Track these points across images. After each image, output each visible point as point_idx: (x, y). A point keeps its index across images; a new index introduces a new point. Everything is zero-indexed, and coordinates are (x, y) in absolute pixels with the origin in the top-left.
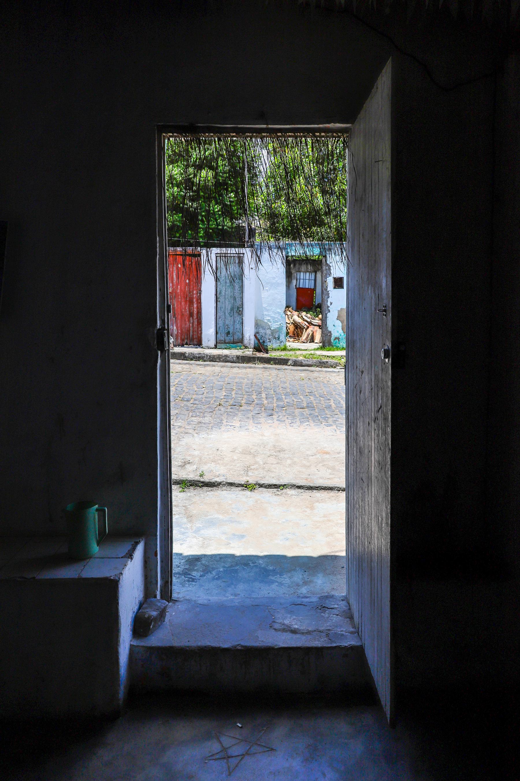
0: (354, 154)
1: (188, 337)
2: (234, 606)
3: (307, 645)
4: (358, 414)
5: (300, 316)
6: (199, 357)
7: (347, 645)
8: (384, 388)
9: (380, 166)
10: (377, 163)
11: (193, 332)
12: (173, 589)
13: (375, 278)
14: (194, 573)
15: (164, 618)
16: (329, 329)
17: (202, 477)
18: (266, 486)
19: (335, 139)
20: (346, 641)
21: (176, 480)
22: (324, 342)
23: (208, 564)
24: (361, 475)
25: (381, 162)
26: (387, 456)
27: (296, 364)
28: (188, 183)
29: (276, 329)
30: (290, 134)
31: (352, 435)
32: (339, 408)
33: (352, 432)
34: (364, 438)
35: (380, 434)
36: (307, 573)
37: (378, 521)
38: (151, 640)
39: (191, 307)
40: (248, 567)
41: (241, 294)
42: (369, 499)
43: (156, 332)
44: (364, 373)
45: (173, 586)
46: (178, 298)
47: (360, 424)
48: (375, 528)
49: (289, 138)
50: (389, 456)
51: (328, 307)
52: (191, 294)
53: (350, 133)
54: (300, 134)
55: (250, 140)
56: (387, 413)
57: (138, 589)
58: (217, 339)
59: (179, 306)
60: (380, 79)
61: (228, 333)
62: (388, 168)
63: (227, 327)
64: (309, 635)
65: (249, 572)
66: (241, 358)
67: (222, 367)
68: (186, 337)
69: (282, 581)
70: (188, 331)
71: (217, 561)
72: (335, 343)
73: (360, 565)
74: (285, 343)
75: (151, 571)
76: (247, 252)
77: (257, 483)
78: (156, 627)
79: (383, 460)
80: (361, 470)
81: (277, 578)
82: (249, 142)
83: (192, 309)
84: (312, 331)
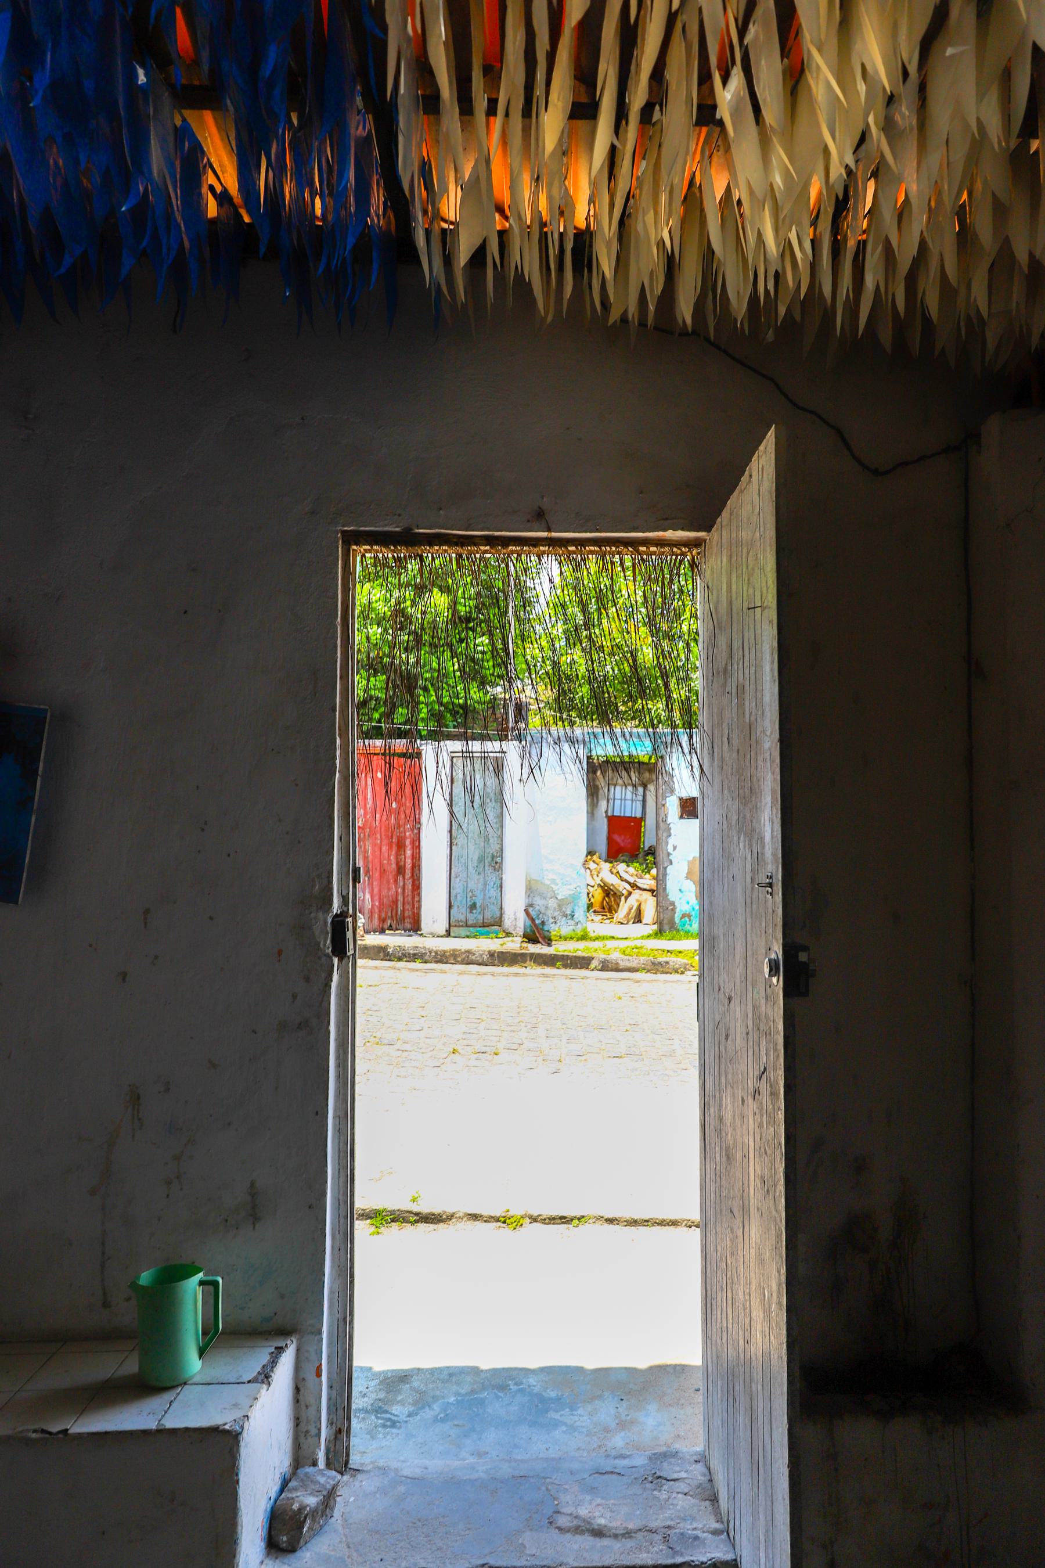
0: (710, 587)
1: (394, 914)
2: (476, 1480)
3: (625, 1563)
4: (724, 1081)
5: (615, 871)
6: (415, 955)
7: (705, 1560)
8: (770, 1034)
9: (758, 616)
10: (753, 610)
11: (404, 904)
12: (351, 1444)
13: (751, 821)
14: (396, 1409)
15: (332, 1510)
16: (671, 898)
17: (415, 1203)
18: (545, 1219)
19: (677, 558)
20: (703, 1551)
21: (363, 1210)
22: (660, 923)
23: (424, 1389)
24: (730, 1203)
25: (759, 609)
26: (778, 1168)
27: (606, 966)
28: (399, 617)
29: (567, 898)
30: (592, 548)
31: (710, 1121)
32: (690, 1056)
33: (713, 1115)
34: (735, 1129)
35: (765, 1123)
36: (624, 1404)
37: (763, 1298)
38: (305, 1561)
39: (401, 855)
40: (506, 1393)
41: (500, 830)
42: (746, 1251)
43: (330, 920)
44: (732, 1002)
45: (351, 1438)
46: (376, 839)
47: (727, 1101)
48: (757, 1313)
49: (590, 556)
50: (781, 1168)
51: (669, 854)
52: (402, 829)
53: (703, 548)
54: (611, 548)
55: (517, 559)
56: (777, 1083)
57: (279, 1449)
58: (452, 918)
59: (378, 853)
60: (755, 460)
61: (473, 907)
62: (771, 622)
63: (471, 894)
64: (627, 1540)
65: (508, 1405)
66: (498, 955)
67: (460, 974)
68: (390, 914)
69: (575, 1422)
70: (393, 902)
71: (443, 1382)
73: (731, 1386)
74: (584, 925)
75: (307, 1407)
76: (512, 749)
77: (526, 1214)
78: (315, 1532)
79: (771, 1176)
80: (729, 1191)
81: (564, 1415)
82: (515, 562)
83: (403, 859)
84: (638, 901)
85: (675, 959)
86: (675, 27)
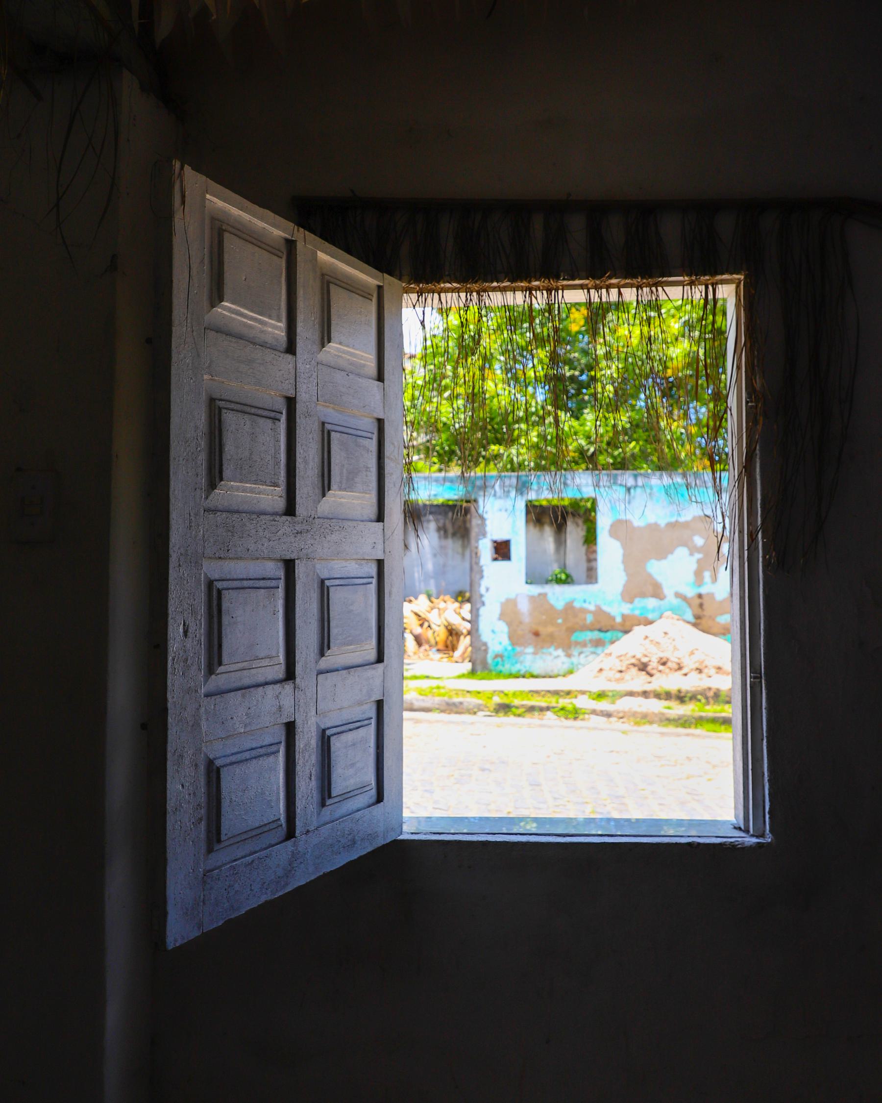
51: (481, 596)
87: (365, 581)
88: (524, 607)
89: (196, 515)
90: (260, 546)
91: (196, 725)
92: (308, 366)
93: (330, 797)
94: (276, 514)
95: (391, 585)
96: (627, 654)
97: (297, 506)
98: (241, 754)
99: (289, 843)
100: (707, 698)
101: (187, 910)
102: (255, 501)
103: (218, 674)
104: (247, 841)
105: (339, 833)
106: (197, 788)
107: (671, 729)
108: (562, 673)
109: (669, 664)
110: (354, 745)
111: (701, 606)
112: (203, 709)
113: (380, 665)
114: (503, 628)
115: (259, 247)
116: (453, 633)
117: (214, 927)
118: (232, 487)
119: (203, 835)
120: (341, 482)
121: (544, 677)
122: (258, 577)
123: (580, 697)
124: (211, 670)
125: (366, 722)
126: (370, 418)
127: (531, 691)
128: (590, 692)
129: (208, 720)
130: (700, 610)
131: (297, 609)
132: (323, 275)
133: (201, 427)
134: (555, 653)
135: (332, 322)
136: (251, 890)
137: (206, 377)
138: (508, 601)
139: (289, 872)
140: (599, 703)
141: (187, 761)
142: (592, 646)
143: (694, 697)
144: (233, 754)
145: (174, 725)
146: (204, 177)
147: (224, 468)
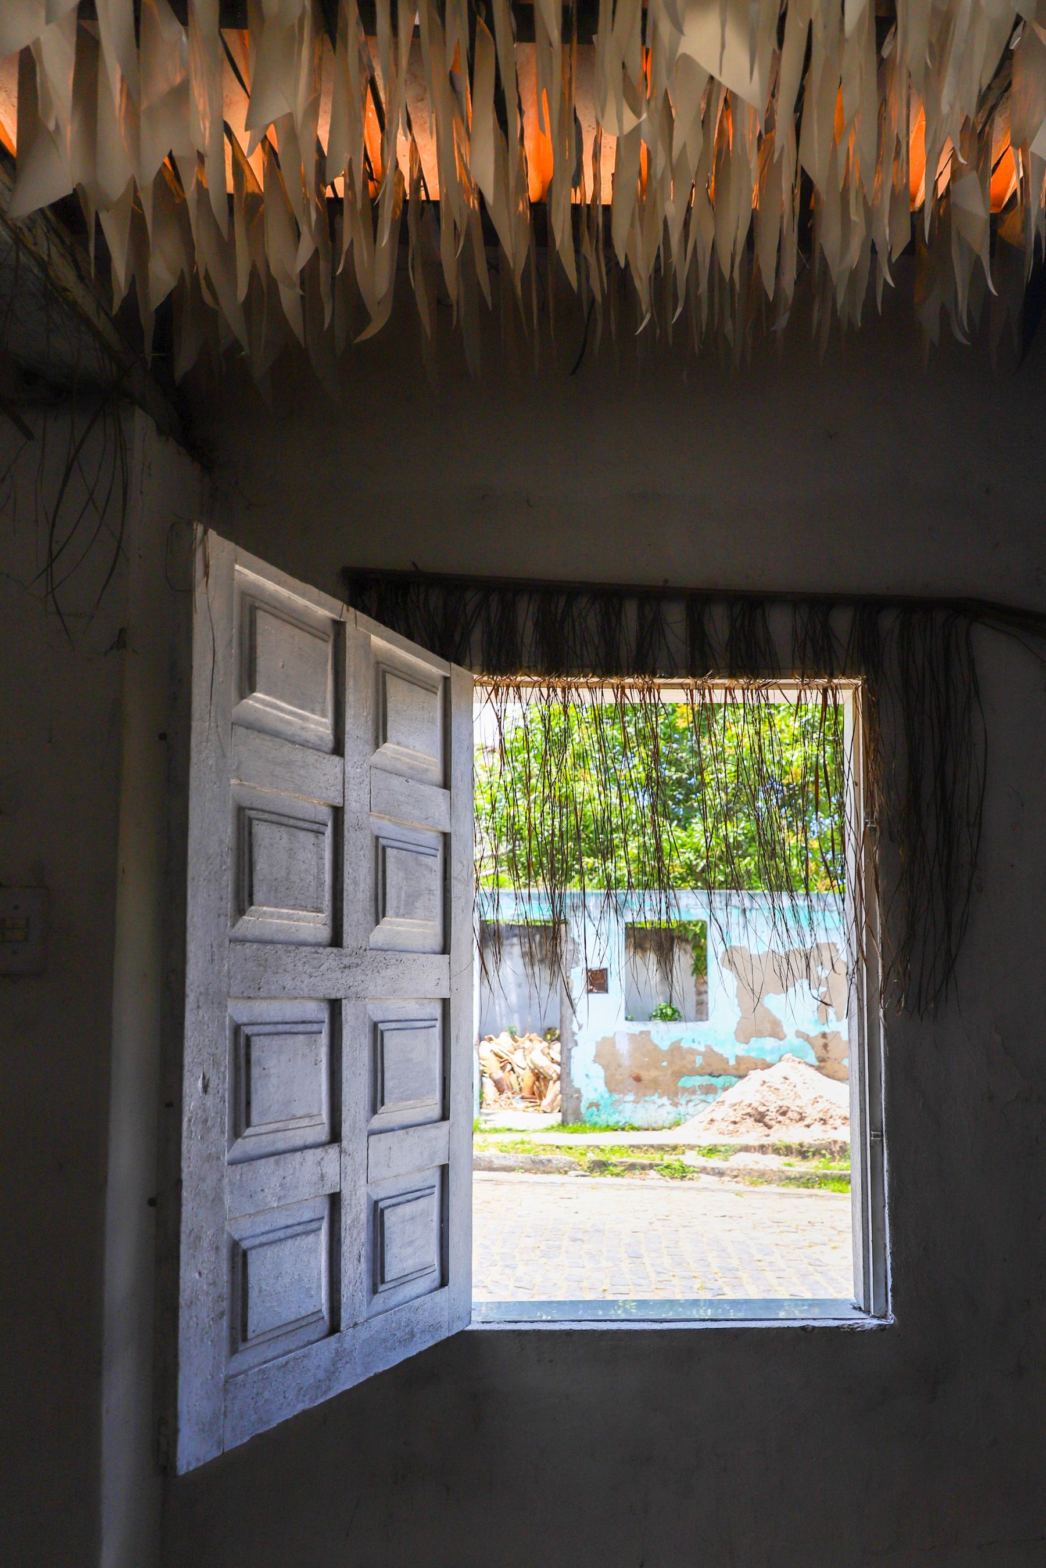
16: (577, 1084)
51: (574, 1034)
72: (589, 1114)
85: (559, 1157)
86: (560, 27)
87: (427, 1024)
88: (623, 1047)
89: (220, 946)
90: (299, 983)
91: (218, 1200)
92: (359, 770)
93: (383, 1282)
94: (318, 945)
95: (459, 1028)
96: (742, 1101)
97: (345, 936)
98: (275, 1233)
99: (333, 1339)
100: (832, 1153)
101: (204, 1425)
102: (293, 930)
103: (246, 1137)
104: (280, 1338)
105: (394, 1325)
106: (218, 1276)
107: (792, 1189)
108: (667, 1124)
109: (790, 1114)
110: (413, 1218)
111: (825, 1046)
112: (226, 1180)
113: (445, 1124)
114: (598, 1073)
115: (300, 629)
116: (539, 1076)
117: (238, 1444)
118: (265, 913)
119: (225, 1333)
120: (398, 907)
121: (647, 1130)
122: (296, 1020)
123: (688, 1153)
124: (236, 1133)
125: (428, 1191)
126: (435, 831)
127: (631, 1146)
128: (700, 1147)
129: (232, 1192)
130: (824, 1052)
131: (344, 1059)
132: (378, 663)
133: (227, 841)
134: (660, 1102)
135: (389, 718)
136: (284, 1397)
137: (233, 781)
138: (604, 1040)
139: (332, 1374)
140: (710, 1160)
141: (205, 1244)
142: (702, 1093)
143: (817, 1152)
144: (263, 1234)
145: (190, 1200)
146: (233, 545)
147: (255, 889)
